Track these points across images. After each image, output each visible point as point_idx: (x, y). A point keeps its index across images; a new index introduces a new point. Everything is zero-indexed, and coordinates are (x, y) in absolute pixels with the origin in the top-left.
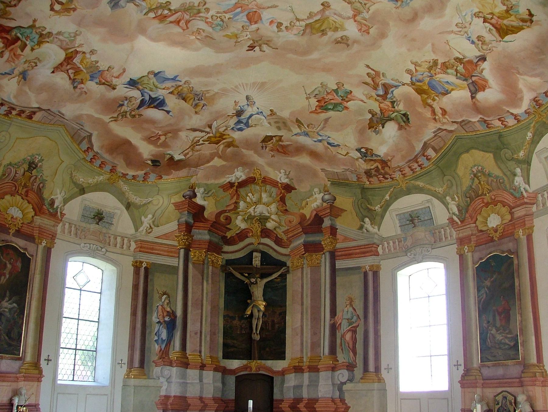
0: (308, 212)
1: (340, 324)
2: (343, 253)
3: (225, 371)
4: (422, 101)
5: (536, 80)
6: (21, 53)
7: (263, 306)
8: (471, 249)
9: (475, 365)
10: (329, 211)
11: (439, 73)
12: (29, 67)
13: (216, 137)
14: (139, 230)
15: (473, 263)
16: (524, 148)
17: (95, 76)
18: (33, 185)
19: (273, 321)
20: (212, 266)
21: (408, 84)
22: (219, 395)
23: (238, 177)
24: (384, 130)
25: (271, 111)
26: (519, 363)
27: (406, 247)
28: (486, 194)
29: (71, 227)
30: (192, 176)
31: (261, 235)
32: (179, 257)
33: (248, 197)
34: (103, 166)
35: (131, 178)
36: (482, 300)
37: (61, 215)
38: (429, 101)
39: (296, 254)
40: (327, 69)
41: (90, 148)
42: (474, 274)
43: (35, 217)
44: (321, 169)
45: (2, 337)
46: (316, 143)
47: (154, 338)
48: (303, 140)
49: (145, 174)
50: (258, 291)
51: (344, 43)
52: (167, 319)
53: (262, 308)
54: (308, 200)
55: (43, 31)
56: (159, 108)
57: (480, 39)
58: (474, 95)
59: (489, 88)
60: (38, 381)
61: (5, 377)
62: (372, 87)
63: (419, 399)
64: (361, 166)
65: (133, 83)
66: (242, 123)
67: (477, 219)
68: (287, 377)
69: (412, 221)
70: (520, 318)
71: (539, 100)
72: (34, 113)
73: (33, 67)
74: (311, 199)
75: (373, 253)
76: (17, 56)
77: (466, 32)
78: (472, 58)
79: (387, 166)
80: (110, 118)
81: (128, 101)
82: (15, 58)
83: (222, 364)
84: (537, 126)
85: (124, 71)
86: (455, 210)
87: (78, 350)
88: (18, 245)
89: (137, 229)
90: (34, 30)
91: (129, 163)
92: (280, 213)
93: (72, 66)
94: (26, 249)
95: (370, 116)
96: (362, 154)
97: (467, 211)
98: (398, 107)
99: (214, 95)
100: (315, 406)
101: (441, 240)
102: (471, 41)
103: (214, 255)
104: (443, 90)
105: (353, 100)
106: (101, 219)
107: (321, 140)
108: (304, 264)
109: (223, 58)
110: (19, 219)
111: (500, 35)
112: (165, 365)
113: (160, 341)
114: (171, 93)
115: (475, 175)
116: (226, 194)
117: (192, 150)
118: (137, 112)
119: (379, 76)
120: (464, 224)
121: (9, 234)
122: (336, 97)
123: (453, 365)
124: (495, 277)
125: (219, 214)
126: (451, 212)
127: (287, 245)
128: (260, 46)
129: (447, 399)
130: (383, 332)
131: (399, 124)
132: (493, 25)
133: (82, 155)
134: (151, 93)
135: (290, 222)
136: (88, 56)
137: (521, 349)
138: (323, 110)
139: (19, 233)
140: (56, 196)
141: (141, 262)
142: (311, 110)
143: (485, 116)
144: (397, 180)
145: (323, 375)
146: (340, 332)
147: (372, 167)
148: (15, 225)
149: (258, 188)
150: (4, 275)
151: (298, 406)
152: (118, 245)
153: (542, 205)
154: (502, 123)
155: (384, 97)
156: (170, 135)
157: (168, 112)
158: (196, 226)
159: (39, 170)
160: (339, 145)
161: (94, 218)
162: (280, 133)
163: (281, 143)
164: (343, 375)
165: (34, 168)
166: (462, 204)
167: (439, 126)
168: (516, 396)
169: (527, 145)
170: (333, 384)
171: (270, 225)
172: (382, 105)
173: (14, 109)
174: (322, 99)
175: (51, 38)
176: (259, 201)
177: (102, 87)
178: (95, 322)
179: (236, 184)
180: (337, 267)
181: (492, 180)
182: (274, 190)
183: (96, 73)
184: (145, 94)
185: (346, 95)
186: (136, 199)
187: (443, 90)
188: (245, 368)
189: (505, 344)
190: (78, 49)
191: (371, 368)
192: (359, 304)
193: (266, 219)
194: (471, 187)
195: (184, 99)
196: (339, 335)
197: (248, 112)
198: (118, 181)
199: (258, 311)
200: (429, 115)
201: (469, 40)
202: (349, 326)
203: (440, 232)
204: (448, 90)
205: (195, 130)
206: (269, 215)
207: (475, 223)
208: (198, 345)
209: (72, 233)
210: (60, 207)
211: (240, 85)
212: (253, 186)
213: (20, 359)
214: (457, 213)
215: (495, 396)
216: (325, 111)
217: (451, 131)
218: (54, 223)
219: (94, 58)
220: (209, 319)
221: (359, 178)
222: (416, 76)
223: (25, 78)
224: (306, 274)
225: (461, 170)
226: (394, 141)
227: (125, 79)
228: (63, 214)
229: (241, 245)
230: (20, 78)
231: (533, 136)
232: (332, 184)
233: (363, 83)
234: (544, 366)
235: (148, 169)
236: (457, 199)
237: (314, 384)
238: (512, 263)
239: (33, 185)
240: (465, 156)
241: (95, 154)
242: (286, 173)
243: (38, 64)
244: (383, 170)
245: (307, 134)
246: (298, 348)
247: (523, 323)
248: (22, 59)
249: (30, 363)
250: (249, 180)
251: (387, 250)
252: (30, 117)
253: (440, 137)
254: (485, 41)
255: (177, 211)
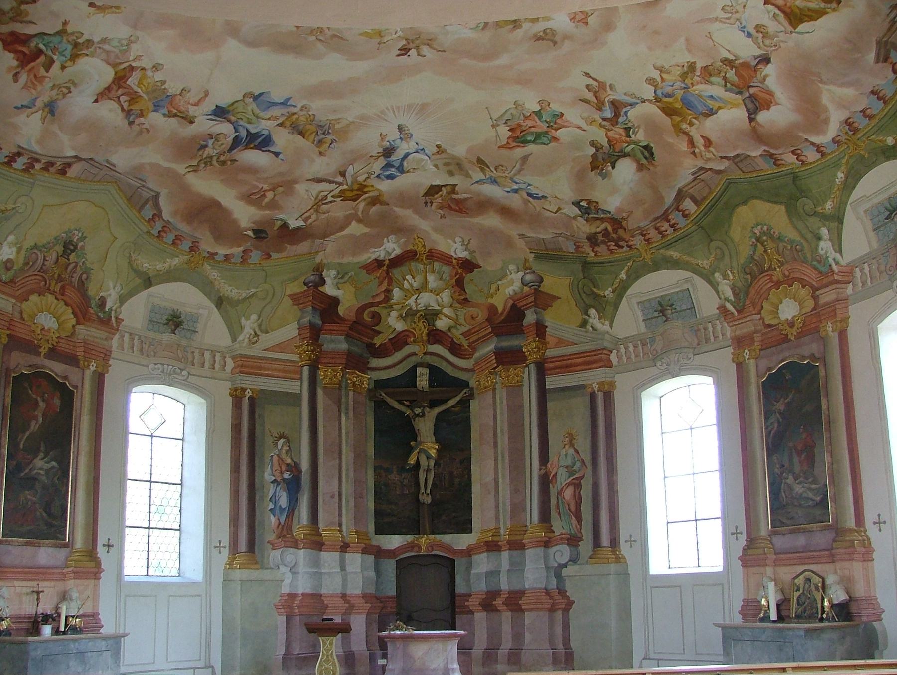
0: (500, 302)
1: (556, 474)
2: (557, 364)
3: (379, 554)
4: (673, 125)
5: (849, 92)
6: (45, 74)
7: (435, 451)
8: (754, 354)
9: (764, 532)
10: (533, 299)
11: (698, 83)
12: (58, 94)
13: (352, 190)
14: (238, 340)
15: (758, 376)
16: (832, 196)
17: (161, 103)
18: (72, 277)
19: (451, 473)
20: (354, 391)
21: (650, 101)
22: (371, 590)
23: (390, 251)
24: (615, 173)
25: (438, 146)
26: (829, 527)
27: (655, 352)
28: (775, 268)
29: (133, 339)
30: (317, 252)
31: (428, 339)
32: (301, 379)
33: (406, 282)
34: (179, 241)
35: (222, 258)
36: (773, 432)
37: (116, 321)
38: (684, 126)
39: (484, 367)
40: (524, 81)
41: (158, 215)
42: (759, 393)
43: (78, 327)
44: (519, 235)
45: (38, 513)
46: (510, 194)
47: (268, 505)
48: (490, 190)
49: (243, 251)
50: (425, 427)
51: (549, 40)
52: (286, 476)
53: (433, 453)
54: (499, 283)
55: (78, 38)
56: (263, 149)
57: (760, 30)
58: (753, 116)
59: (777, 104)
60: (95, 579)
61: (46, 573)
62: (595, 105)
63: (680, 587)
64: (580, 229)
65: (220, 112)
66: (393, 166)
67: (762, 307)
68: (475, 558)
69: (662, 312)
70: (829, 458)
71: (853, 122)
72: (69, 165)
73: (64, 95)
74: (504, 281)
75: (602, 364)
76: (39, 79)
77: (737, 20)
78: (749, 60)
79: (622, 227)
80: (187, 168)
81: (213, 140)
82: (36, 83)
83: (374, 543)
84: (851, 161)
85: (207, 94)
86: (729, 294)
87: (152, 528)
88: (53, 371)
89: (234, 340)
90: (65, 38)
91: (219, 236)
92: (457, 305)
93: (126, 90)
94: (66, 378)
95: (593, 150)
96: (583, 211)
97: (747, 294)
98: (635, 136)
99: (348, 125)
100: (520, 602)
101: (707, 340)
102: (746, 33)
103: (356, 374)
104: (705, 108)
105: (566, 127)
106: (178, 325)
107: (517, 189)
108: (496, 383)
109: (361, 67)
110: (52, 331)
111: (791, 24)
112: (286, 547)
113: (277, 511)
114: (281, 125)
115: (758, 240)
116: (372, 277)
117: (317, 211)
118: (228, 156)
119: (605, 90)
120: (742, 316)
121: (40, 355)
122: (539, 122)
123: (729, 534)
124: (791, 396)
125: (361, 310)
126: (722, 297)
127: (470, 354)
128: (417, 48)
129: (722, 585)
130: (621, 487)
131: (638, 162)
132: (780, 9)
133: (145, 227)
134: (249, 126)
135: (473, 318)
136: (149, 73)
137: (831, 506)
138: (519, 143)
139: (54, 353)
140: (109, 293)
141: (244, 390)
142: (499, 144)
143: (772, 148)
144: (638, 249)
145: (531, 554)
146: (556, 487)
147: (598, 230)
148: (48, 341)
149: (421, 266)
150: (35, 418)
151: (494, 603)
152: (207, 364)
153: (860, 285)
154: (797, 159)
155: (614, 121)
156: (281, 189)
157: (277, 154)
158: (326, 330)
159: (79, 253)
160: (544, 197)
161: (167, 324)
162: (452, 181)
163: (454, 196)
164: (561, 553)
165: (73, 251)
166: (739, 285)
167: (700, 163)
168: (825, 576)
169: (838, 192)
170: (547, 568)
171: (441, 324)
172: (610, 134)
173: (38, 161)
174: (516, 126)
175: (91, 50)
176: (423, 288)
177: (173, 120)
178: (176, 484)
179: (387, 262)
180: (547, 387)
181: (785, 247)
182: (446, 270)
183: (162, 100)
184: (241, 129)
185: (554, 119)
186: (231, 291)
187: (705, 108)
188: (411, 546)
189: (808, 498)
190: (134, 64)
191: (605, 540)
192: (583, 444)
193: (436, 314)
194: (752, 257)
195: (302, 134)
196: (553, 491)
197: (401, 150)
198: (202, 265)
199: (428, 458)
200: (684, 147)
201: (744, 32)
202: (569, 477)
203: (705, 329)
204: (712, 109)
205: (319, 181)
206: (439, 308)
207: (759, 313)
208: (337, 513)
209: (135, 348)
210: (114, 308)
211: (388, 109)
212: (413, 264)
213: (66, 546)
214: (732, 298)
215: (794, 578)
216: (522, 145)
217: (719, 172)
218: (107, 334)
219: (159, 76)
220: (352, 474)
221: (578, 247)
222: (662, 88)
223: (52, 112)
224: (501, 398)
225: (736, 232)
226: (631, 189)
227: (209, 106)
228: (119, 319)
229: (399, 355)
230: (45, 113)
231: (846, 178)
232: (536, 257)
233: (580, 100)
234: (865, 531)
235: (249, 244)
236: (731, 278)
237: (517, 568)
238: (816, 376)
239: (72, 277)
240: (742, 210)
241: (165, 224)
242: (463, 241)
243: (73, 89)
244: (616, 233)
245: (495, 181)
246: (492, 513)
247: (835, 466)
248: (48, 84)
249: (81, 552)
250: (406, 256)
251: (625, 359)
252: (63, 172)
253: (703, 181)
254: (767, 33)
255: (296, 307)
